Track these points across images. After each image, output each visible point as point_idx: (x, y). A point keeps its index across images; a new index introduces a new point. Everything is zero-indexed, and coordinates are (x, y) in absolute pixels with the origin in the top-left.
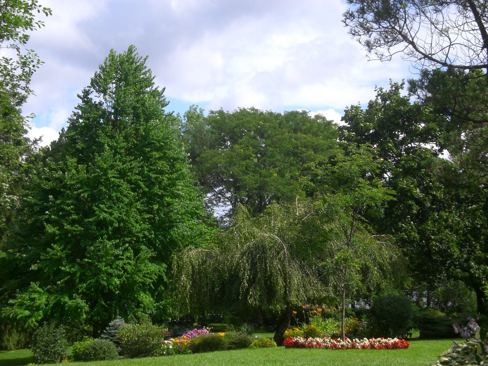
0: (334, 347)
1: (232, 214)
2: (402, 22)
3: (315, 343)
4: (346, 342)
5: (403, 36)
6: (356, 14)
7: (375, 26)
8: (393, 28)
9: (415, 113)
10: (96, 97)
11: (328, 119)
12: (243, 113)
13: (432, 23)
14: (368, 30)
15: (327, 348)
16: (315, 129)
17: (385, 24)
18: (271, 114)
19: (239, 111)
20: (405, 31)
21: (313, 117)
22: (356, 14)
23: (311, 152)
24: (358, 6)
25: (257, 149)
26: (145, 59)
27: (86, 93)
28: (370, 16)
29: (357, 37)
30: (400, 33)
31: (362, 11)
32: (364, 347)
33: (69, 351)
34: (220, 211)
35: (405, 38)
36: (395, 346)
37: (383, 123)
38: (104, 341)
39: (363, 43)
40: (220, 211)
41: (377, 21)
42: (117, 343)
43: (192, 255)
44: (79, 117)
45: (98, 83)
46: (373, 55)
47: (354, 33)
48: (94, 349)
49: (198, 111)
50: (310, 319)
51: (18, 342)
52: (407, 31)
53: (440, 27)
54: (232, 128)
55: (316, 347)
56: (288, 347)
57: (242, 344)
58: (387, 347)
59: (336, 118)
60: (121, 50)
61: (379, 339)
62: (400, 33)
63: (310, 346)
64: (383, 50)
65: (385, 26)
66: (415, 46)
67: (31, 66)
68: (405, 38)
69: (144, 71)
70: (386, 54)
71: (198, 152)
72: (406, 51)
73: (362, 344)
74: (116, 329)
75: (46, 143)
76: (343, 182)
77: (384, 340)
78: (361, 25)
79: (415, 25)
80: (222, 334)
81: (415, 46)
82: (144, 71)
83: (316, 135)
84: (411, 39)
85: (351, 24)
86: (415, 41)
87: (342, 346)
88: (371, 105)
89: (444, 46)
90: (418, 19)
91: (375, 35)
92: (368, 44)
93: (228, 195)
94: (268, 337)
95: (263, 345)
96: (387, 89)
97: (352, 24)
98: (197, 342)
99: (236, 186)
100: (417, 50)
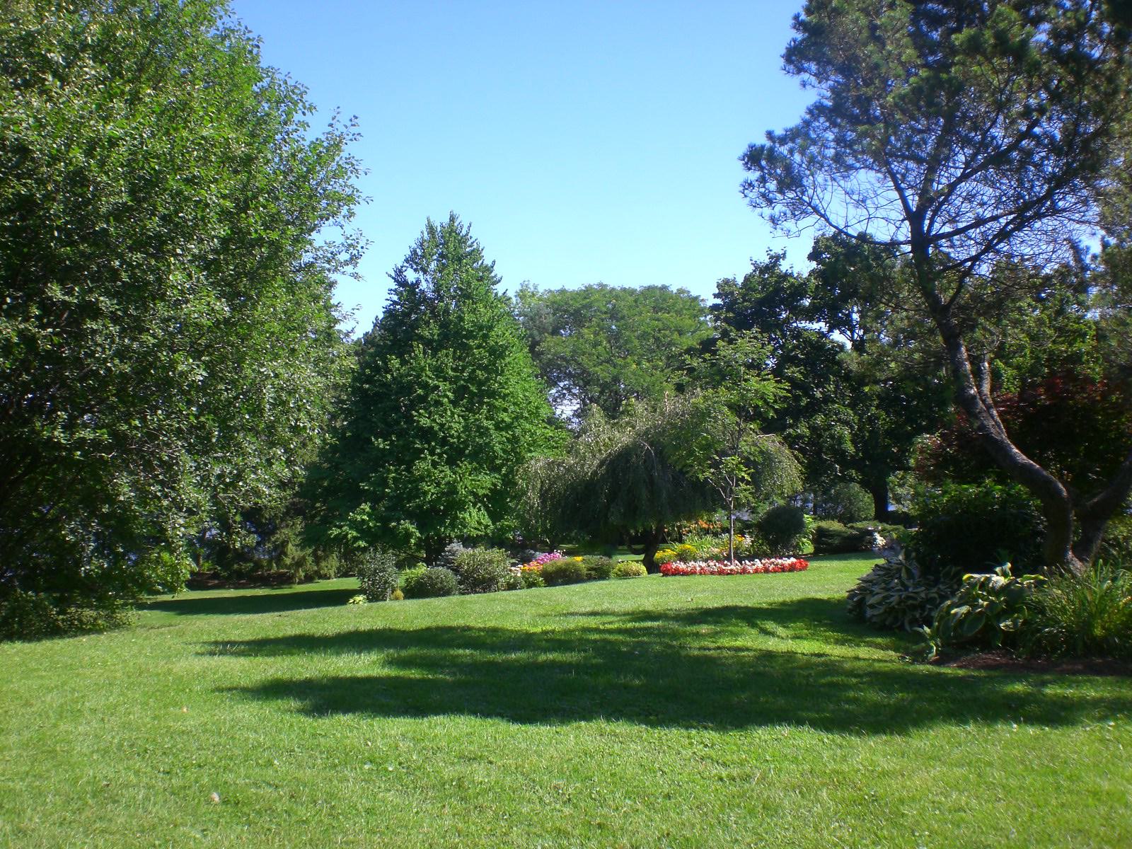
0: (721, 572)
1: (581, 414)
2: (810, 192)
3: (698, 569)
4: (735, 566)
5: (813, 208)
6: (756, 184)
7: (779, 196)
8: (801, 198)
9: (799, 289)
10: (411, 276)
11: (694, 294)
12: (587, 292)
13: (847, 193)
14: (770, 202)
15: (712, 573)
16: (678, 307)
17: (791, 195)
18: (624, 290)
19: (326, 235)
20: (816, 201)
21: (675, 291)
22: (756, 184)
23: (676, 336)
24: (758, 174)
25: (595, 334)
26: (469, 227)
27: (399, 272)
28: (772, 185)
29: (758, 210)
30: (809, 204)
31: (763, 180)
32: (756, 571)
33: (400, 581)
34: (567, 409)
35: (816, 210)
36: (792, 568)
37: (760, 302)
38: (440, 568)
39: (767, 218)
40: (567, 409)
41: (781, 191)
42: (456, 571)
43: (538, 461)
44: (395, 303)
45: (414, 260)
46: (779, 232)
47: (755, 206)
48: (430, 578)
49: (531, 286)
50: (684, 537)
51: (338, 569)
52: (818, 202)
53: (855, 197)
54: (572, 311)
55: (701, 574)
56: (666, 574)
57: (600, 574)
58: (783, 569)
59: (708, 295)
60: (440, 220)
61: (773, 560)
62: (809, 204)
63: (693, 573)
64: (790, 224)
65: (792, 196)
66: (827, 220)
67: (359, 248)
68: (816, 210)
69: (469, 243)
70: (794, 229)
71: (538, 338)
72: (817, 226)
73: (754, 567)
74: (453, 555)
75: (358, 335)
76: (721, 375)
77: (780, 561)
78: (763, 195)
79: (827, 196)
80: (579, 559)
81: (827, 220)
82: (469, 243)
83: (679, 313)
84: (822, 212)
85: (751, 195)
86: (828, 214)
87: (731, 570)
88: (747, 279)
89: (862, 218)
90: (829, 188)
91: (779, 208)
92: (773, 220)
93: (576, 391)
94: (633, 562)
95: (625, 575)
96: (764, 260)
97: (753, 194)
98: (550, 569)
99: (584, 380)
100: (831, 224)
